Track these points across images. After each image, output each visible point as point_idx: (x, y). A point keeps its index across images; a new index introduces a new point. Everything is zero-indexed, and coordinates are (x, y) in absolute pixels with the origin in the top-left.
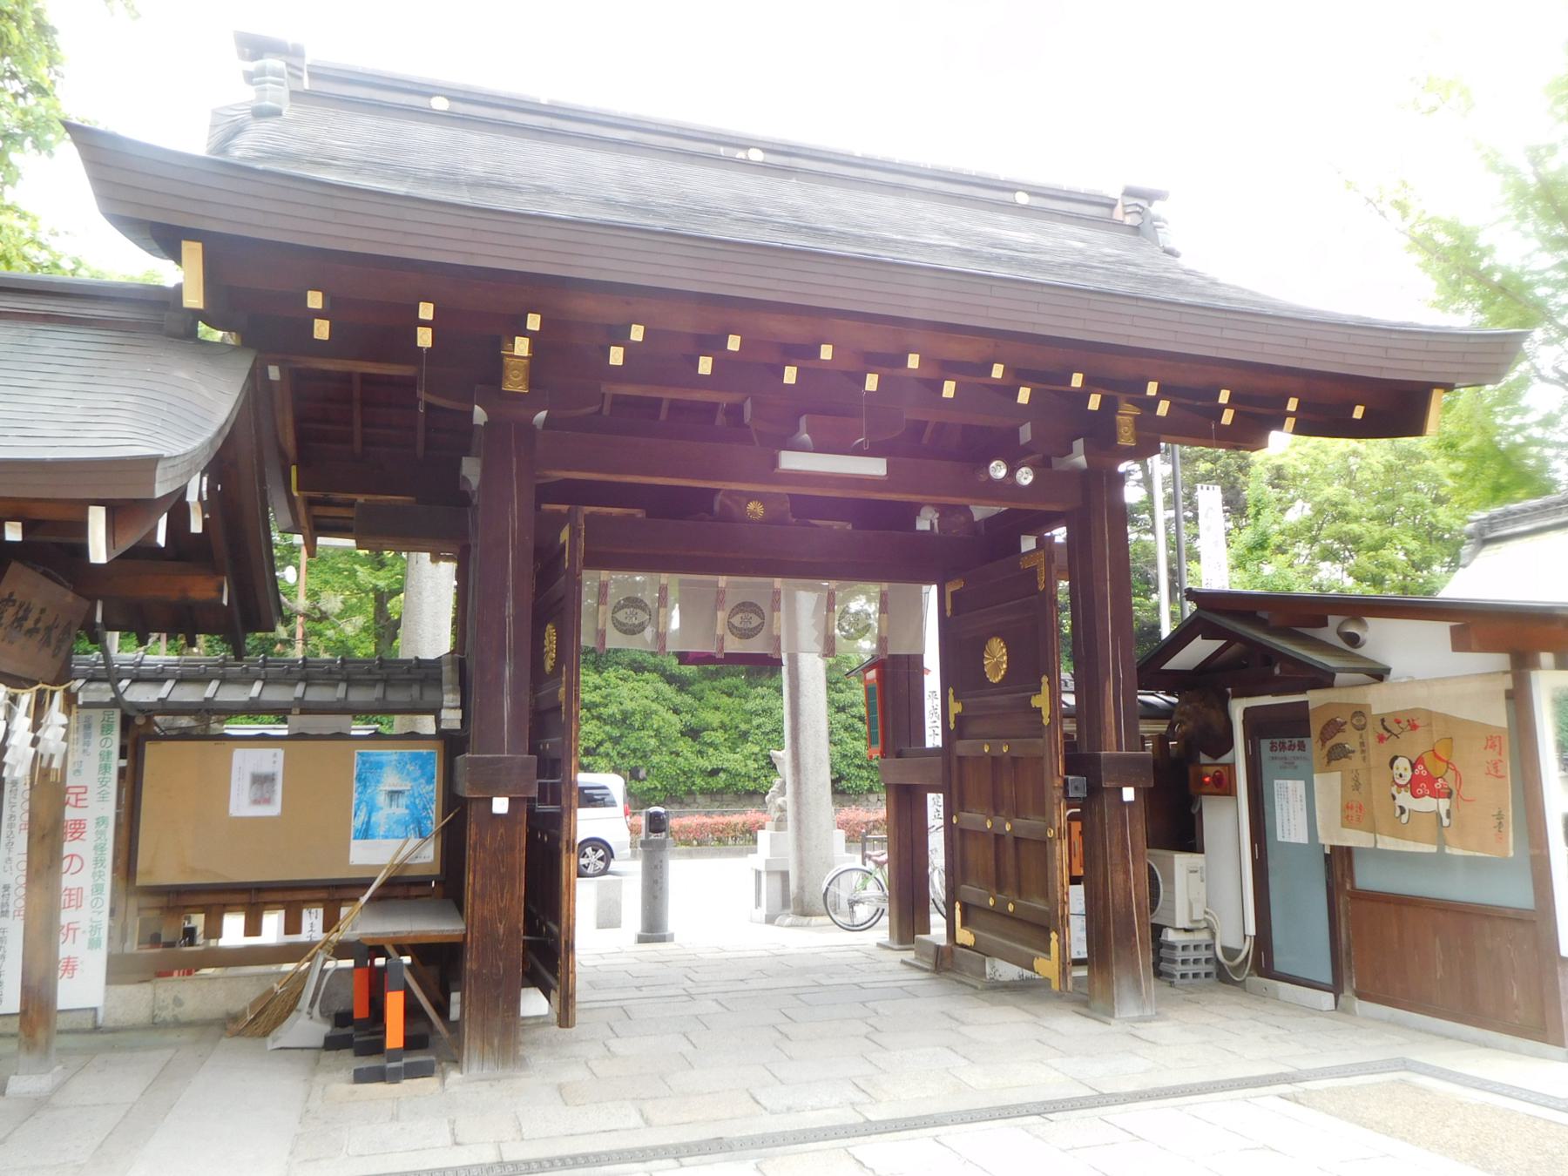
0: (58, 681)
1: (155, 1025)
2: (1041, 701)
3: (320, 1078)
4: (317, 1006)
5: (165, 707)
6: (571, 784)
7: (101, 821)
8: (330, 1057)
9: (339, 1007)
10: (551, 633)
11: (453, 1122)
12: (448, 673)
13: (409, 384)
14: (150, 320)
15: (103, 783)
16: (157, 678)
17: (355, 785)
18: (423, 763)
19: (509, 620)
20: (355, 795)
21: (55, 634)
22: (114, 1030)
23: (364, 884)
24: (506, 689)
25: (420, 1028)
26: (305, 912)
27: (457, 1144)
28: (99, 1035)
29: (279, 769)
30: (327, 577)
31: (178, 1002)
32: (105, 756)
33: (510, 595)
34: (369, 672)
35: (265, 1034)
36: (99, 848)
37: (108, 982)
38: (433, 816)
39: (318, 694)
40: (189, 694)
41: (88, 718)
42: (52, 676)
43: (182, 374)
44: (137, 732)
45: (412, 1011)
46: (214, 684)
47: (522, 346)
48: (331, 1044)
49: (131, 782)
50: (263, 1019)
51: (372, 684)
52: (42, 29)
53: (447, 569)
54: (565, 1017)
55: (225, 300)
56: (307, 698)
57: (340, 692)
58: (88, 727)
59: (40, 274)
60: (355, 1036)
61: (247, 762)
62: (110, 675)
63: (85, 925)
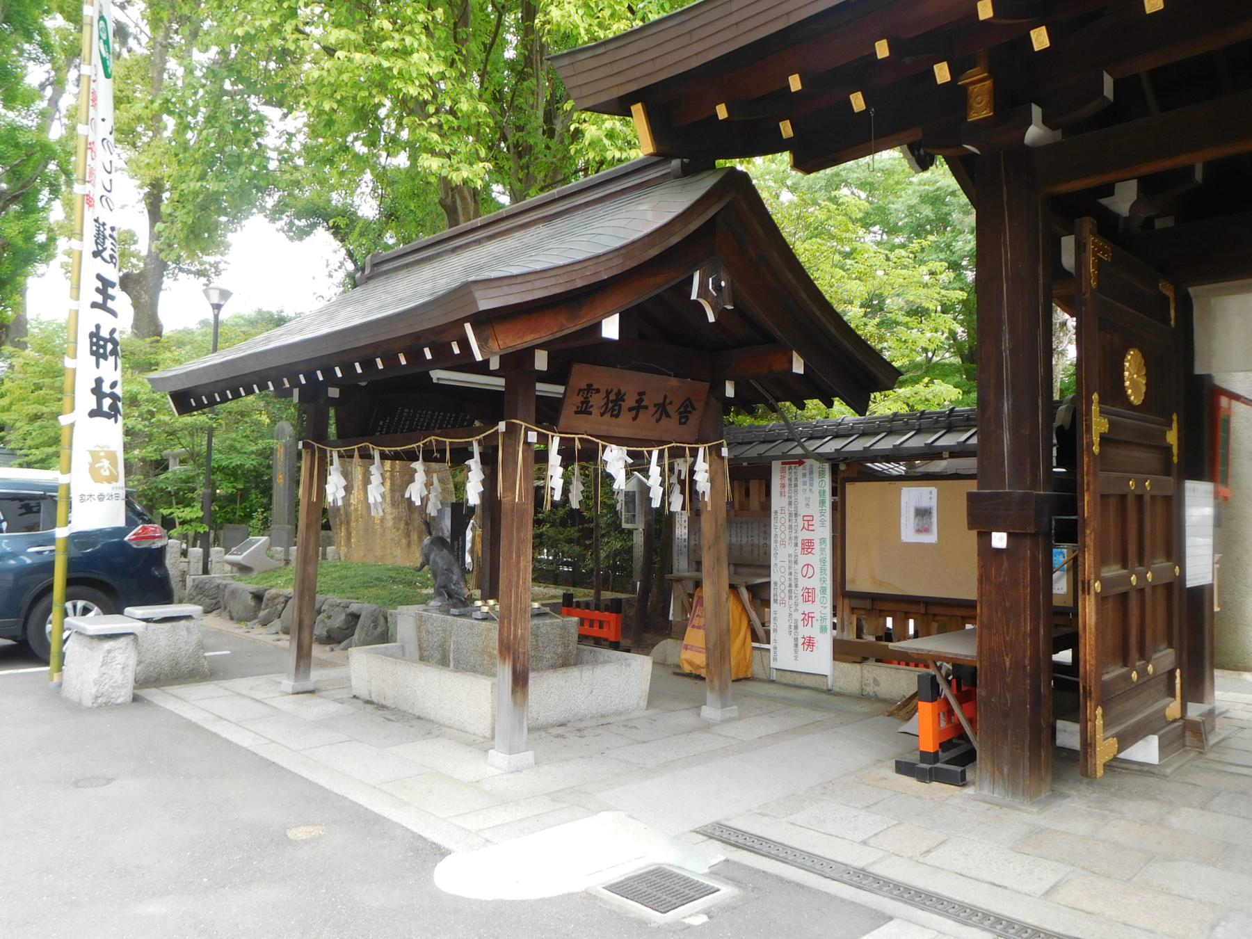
1: (862, 697)
2: (974, 441)
7: (823, 541)
15: (822, 513)
19: (1006, 354)
29: (933, 504)
31: (876, 683)
32: (822, 493)
33: (1006, 328)
36: (823, 561)
37: (834, 659)
49: (839, 510)
58: (811, 472)
63: (817, 615)
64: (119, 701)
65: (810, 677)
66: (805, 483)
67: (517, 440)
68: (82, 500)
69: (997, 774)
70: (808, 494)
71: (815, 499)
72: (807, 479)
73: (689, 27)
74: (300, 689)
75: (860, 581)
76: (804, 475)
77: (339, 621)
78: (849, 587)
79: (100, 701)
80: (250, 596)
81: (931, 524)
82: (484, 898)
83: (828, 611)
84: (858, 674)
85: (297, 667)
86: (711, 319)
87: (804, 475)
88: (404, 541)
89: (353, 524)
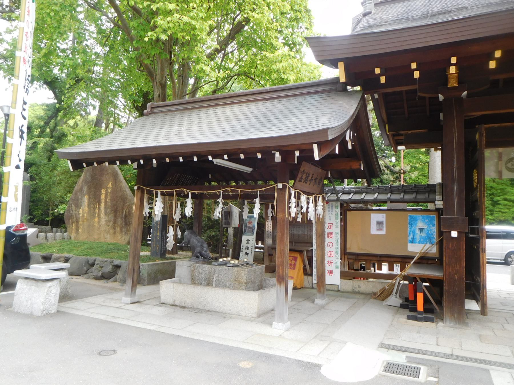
0: (320, 194)
1: (354, 292)
3: (398, 316)
4: (398, 294)
5: (351, 201)
6: (483, 229)
7: (337, 233)
8: (402, 310)
9: (406, 296)
10: (475, 173)
11: (437, 338)
12: (438, 189)
13: (415, 91)
14: (333, 88)
15: (337, 222)
16: (349, 193)
17: (408, 226)
18: (432, 219)
19: (455, 169)
20: (408, 229)
21: (317, 181)
22: (342, 292)
23: (412, 258)
24: (455, 194)
25: (428, 307)
26: (395, 265)
27: (438, 345)
28: (338, 292)
30: (411, 159)
31: (359, 287)
32: (337, 215)
33: (455, 160)
34: (411, 189)
35: (383, 300)
36: (337, 241)
38: (435, 237)
39: (394, 197)
40: (357, 197)
41: (332, 204)
42: (318, 192)
43: (341, 102)
44: (345, 208)
45: (426, 300)
46: (364, 194)
47: (453, 70)
48: (402, 306)
50: (382, 296)
51: (412, 193)
52: (307, 11)
53: (439, 153)
54: (483, 311)
55: (353, 77)
56: (391, 198)
57: (402, 196)
58: (332, 207)
59: (311, 81)
60: (408, 305)
61: (375, 217)
62: (335, 192)
63: (334, 262)
64: (53, 312)
65: (329, 286)
66: (329, 211)
67: (285, 191)
68: (11, 211)
69: (452, 317)
70: (330, 215)
71: (334, 217)
72: (330, 209)
73: (381, 38)
74: (133, 302)
75: (353, 248)
76: (329, 208)
77: (108, 268)
78: (348, 251)
79: (44, 312)
80: (40, 258)
81: (383, 227)
82: (366, 380)
83: (339, 261)
84: (352, 284)
85: (132, 291)
86: (350, 147)
87: (329, 208)
88: (112, 231)
89: (80, 223)
